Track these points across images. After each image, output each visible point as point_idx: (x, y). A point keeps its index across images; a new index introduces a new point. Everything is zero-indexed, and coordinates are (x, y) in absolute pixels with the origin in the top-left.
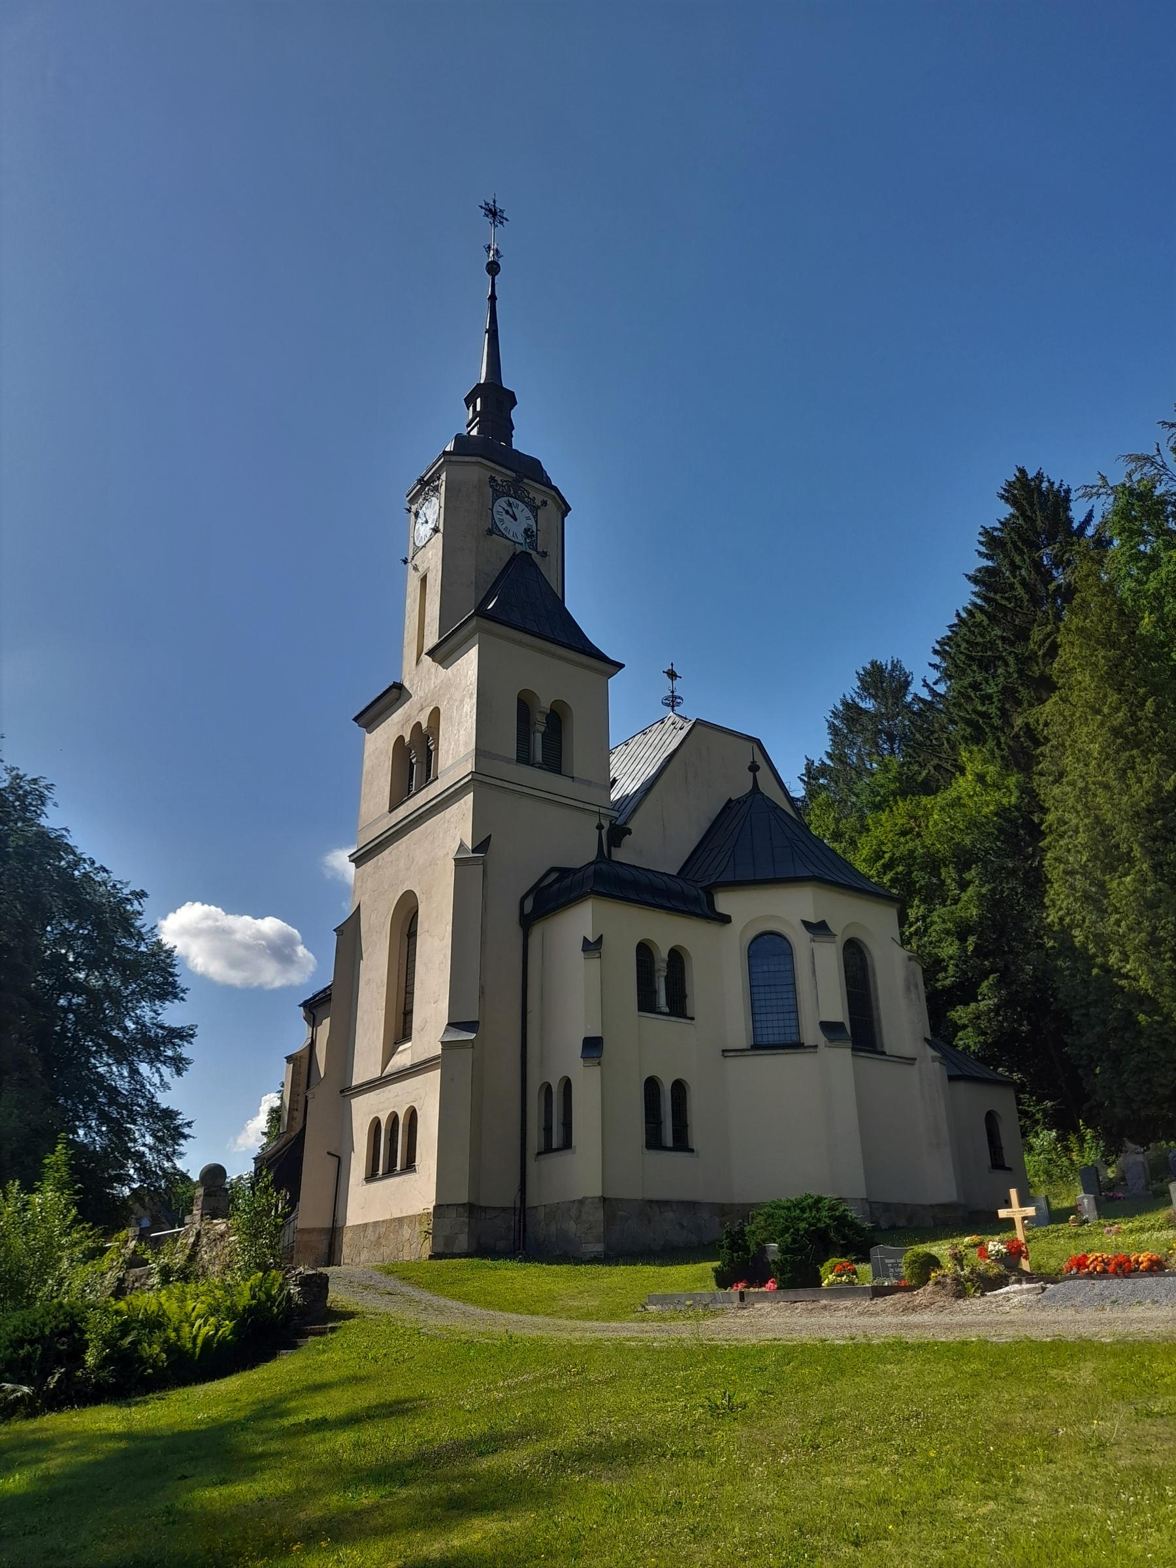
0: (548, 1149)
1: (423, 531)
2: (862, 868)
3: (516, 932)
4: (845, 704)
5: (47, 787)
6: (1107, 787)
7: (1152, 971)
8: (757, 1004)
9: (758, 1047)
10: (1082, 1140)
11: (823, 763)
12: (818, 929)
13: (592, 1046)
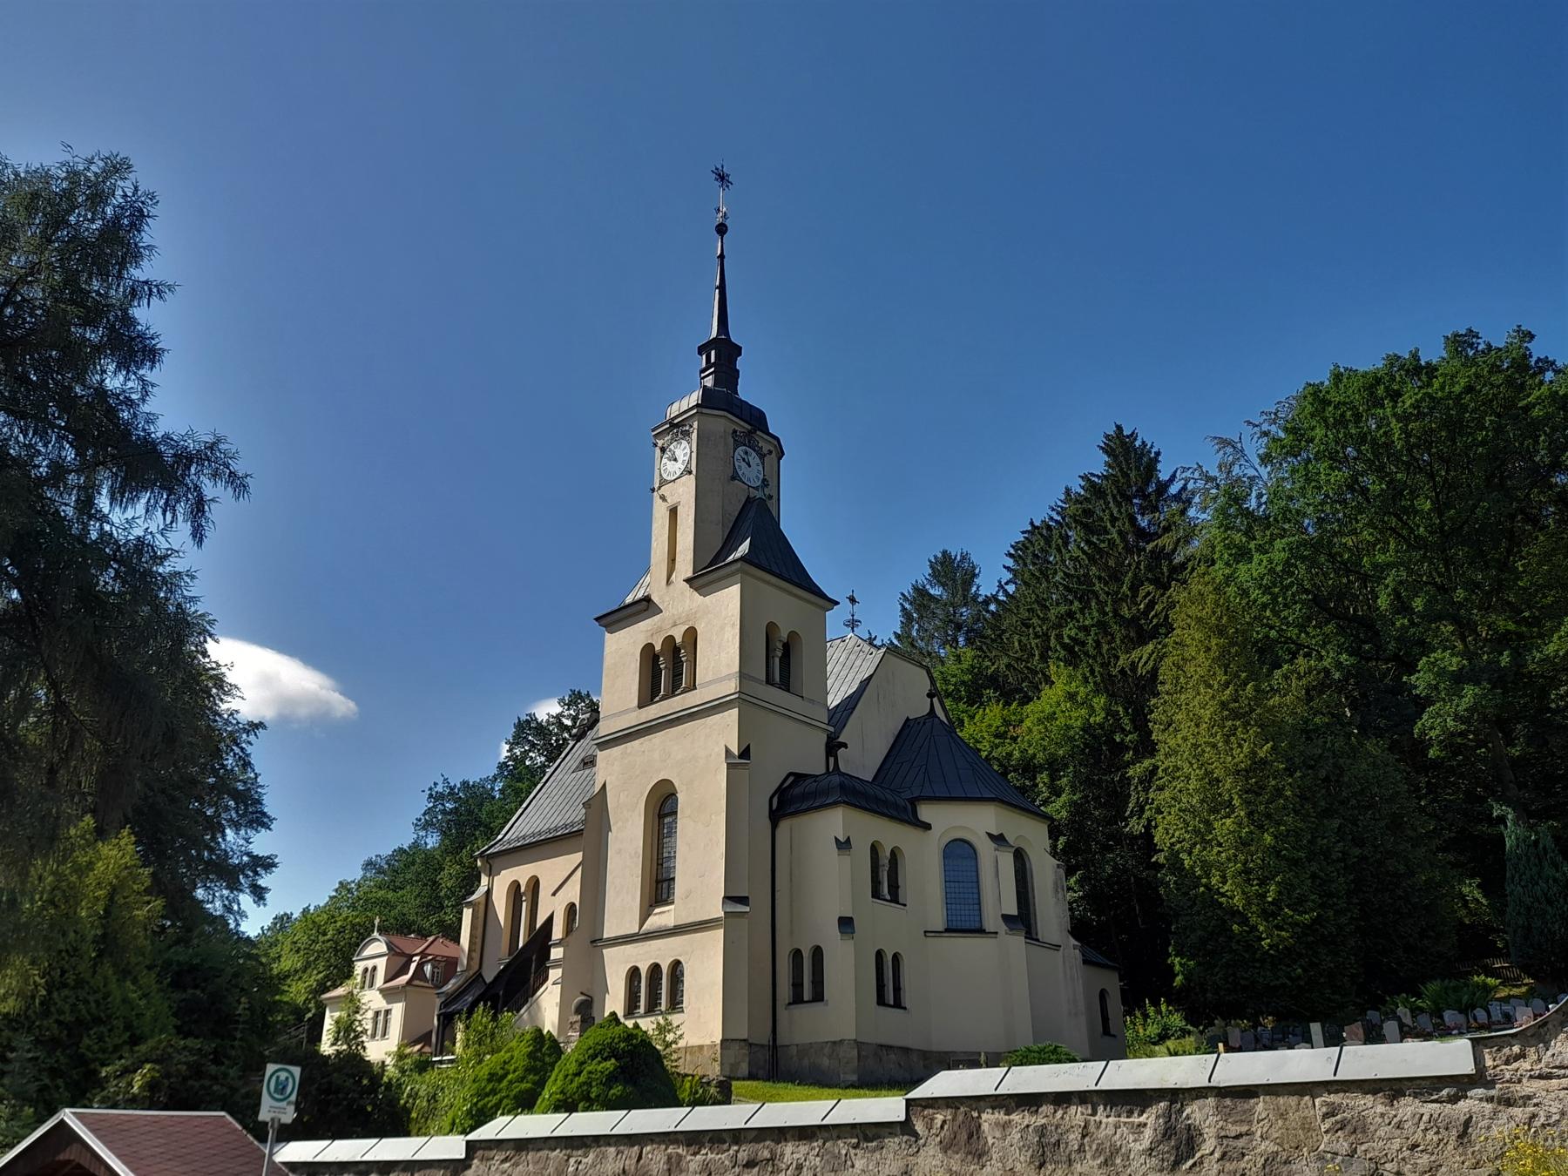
0: (797, 999)
4: (915, 588)
5: (209, 622)
7: (1244, 893)
9: (947, 930)
10: (1146, 1016)
12: (999, 839)
13: (846, 924)
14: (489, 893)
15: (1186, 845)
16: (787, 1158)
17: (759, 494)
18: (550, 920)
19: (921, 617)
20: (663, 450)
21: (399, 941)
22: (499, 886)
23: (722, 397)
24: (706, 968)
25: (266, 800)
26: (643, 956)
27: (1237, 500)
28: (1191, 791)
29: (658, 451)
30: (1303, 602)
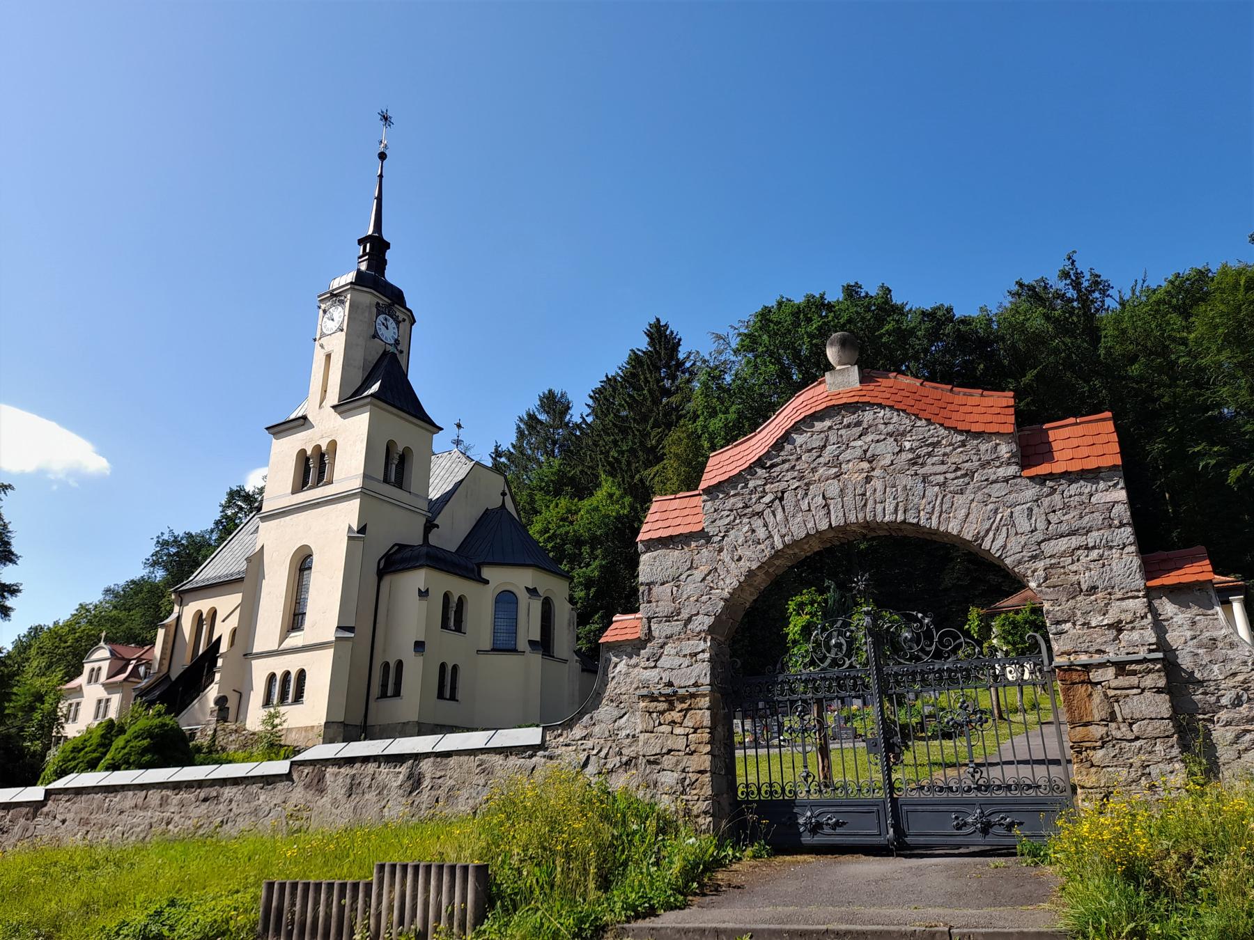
0: (384, 695)
1: (330, 326)
2: (536, 536)
3: (376, 578)
8: (1008, 756)
9: (493, 650)
12: (533, 592)
13: (419, 646)
14: (179, 618)
16: (225, 796)
17: (392, 349)
18: (220, 638)
20: (325, 312)
21: (121, 650)
22: (188, 613)
23: (373, 278)
24: (320, 672)
25: (13, 541)
26: (279, 666)
29: (321, 312)
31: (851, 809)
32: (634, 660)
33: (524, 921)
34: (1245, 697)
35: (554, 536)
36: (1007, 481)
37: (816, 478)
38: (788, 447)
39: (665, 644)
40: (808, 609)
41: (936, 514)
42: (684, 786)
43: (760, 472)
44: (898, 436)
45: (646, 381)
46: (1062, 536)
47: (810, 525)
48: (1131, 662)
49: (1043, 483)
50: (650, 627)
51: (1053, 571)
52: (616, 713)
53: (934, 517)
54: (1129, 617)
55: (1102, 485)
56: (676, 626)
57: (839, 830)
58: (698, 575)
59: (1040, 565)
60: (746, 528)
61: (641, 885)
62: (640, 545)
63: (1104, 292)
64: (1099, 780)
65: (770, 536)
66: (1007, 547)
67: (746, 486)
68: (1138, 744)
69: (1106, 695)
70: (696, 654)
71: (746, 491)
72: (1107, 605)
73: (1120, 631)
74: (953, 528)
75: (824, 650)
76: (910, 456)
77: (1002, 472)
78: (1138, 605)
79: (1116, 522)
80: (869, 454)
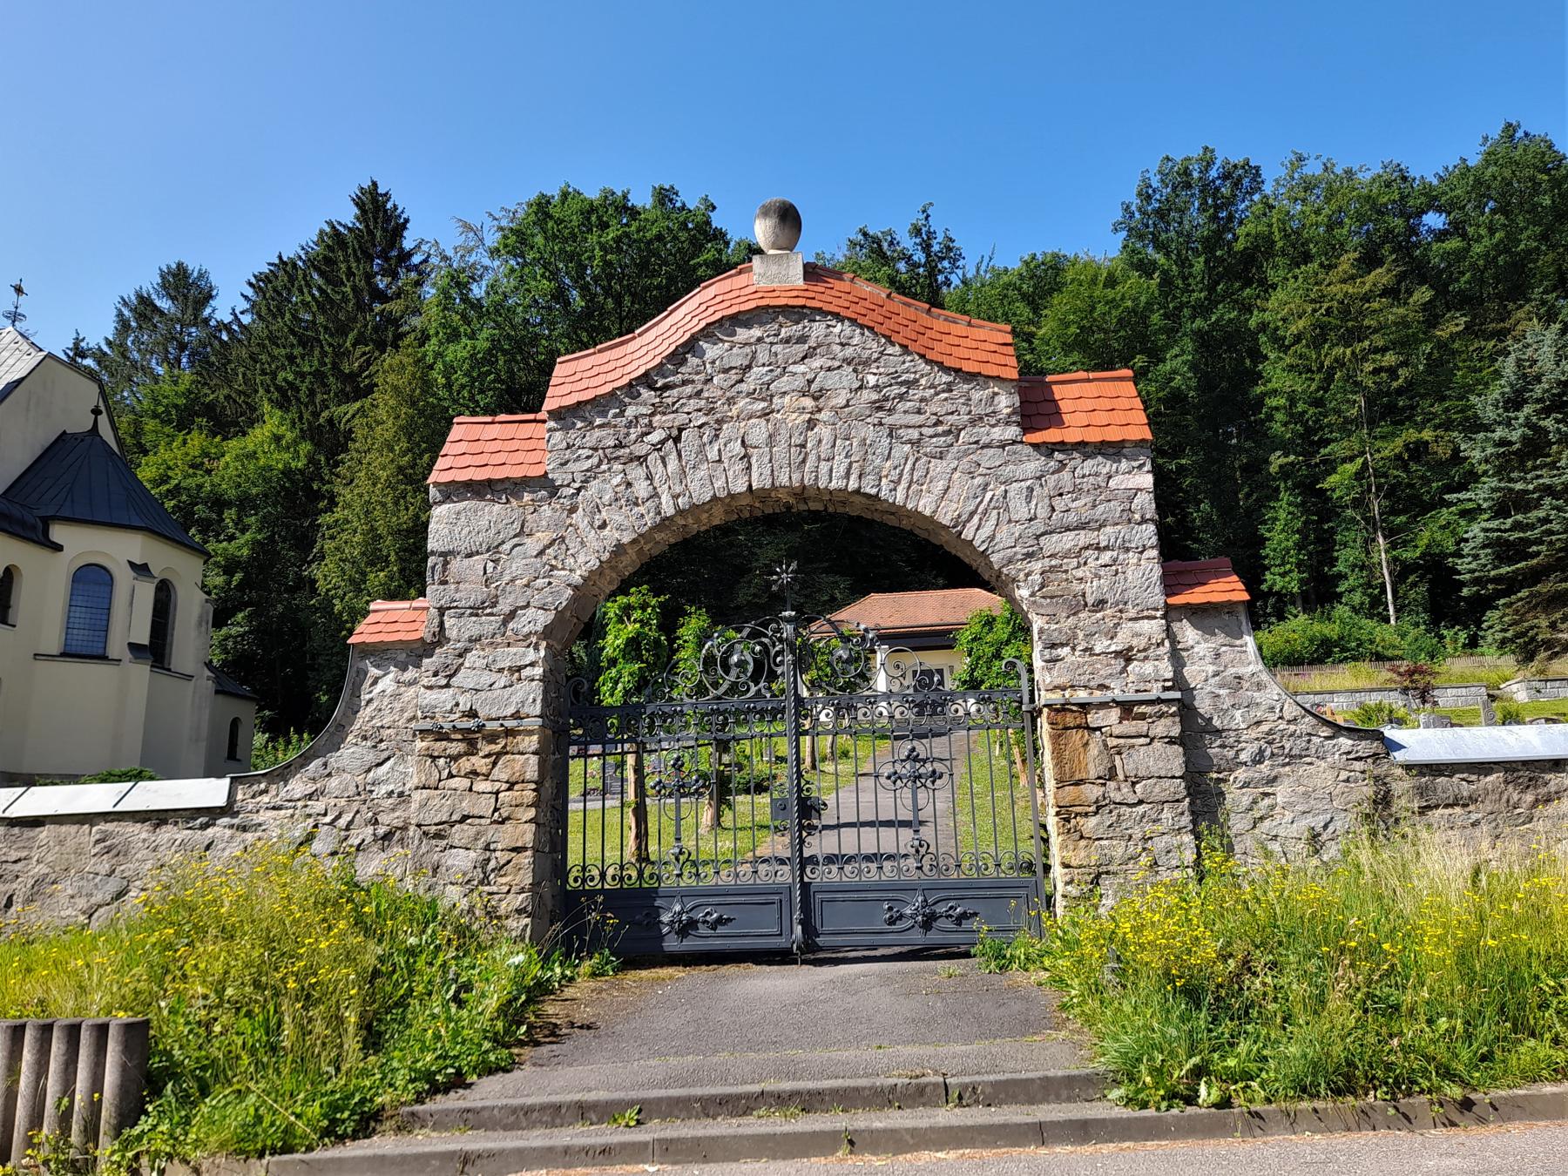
4: (140, 297)
6: (384, 505)
9: (63, 655)
10: (288, 742)
11: (100, 349)
12: (141, 570)
15: (340, 592)
19: (140, 327)
27: (462, 286)
28: (354, 543)
30: (495, 389)
31: (743, 899)
32: (411, 673)
33: (223, 1113)
34: (1268, 753)
35: (175, 492)
36: (1003, 447)
37: (734, 412)
38: (693, 361)
39: (467, 650)
40: (637, 614)
41: (904, 484)
42: (485, 872)
43: (646, 394)
44: (859, 364)
45: (350, 274)
46: (1068, 529)
47: (719, 484)
48: (1142, 703)
49: (1050, 455)
50: (442, 624)
51: (1052, 576)
52: (371, 757)
53: (900, 489)
54: (1143, 643)
55: (1124, 465)
56: (488, 624)
57: (721, 930)
58: (532, 545)
59: (1037, 566)
60: (617, 480)
61: (437, 1037)
62: (432, 490)
63: (954, 261)
64: (1088, 856)
65: (655, 495)
66: (991, 537)
67: (622, 414)
68: (1141, 809)
69: (1106, 745)
70: (519, 669)
71: (622, 421)
72: (1117, 625)
73: (1129, 660)
74: (925, 506)
75: (720, 671)
76: (875, 396)
77: (998, 434)
78: (1154, 628)
79: (1137, 517)
80: (814, 387)
